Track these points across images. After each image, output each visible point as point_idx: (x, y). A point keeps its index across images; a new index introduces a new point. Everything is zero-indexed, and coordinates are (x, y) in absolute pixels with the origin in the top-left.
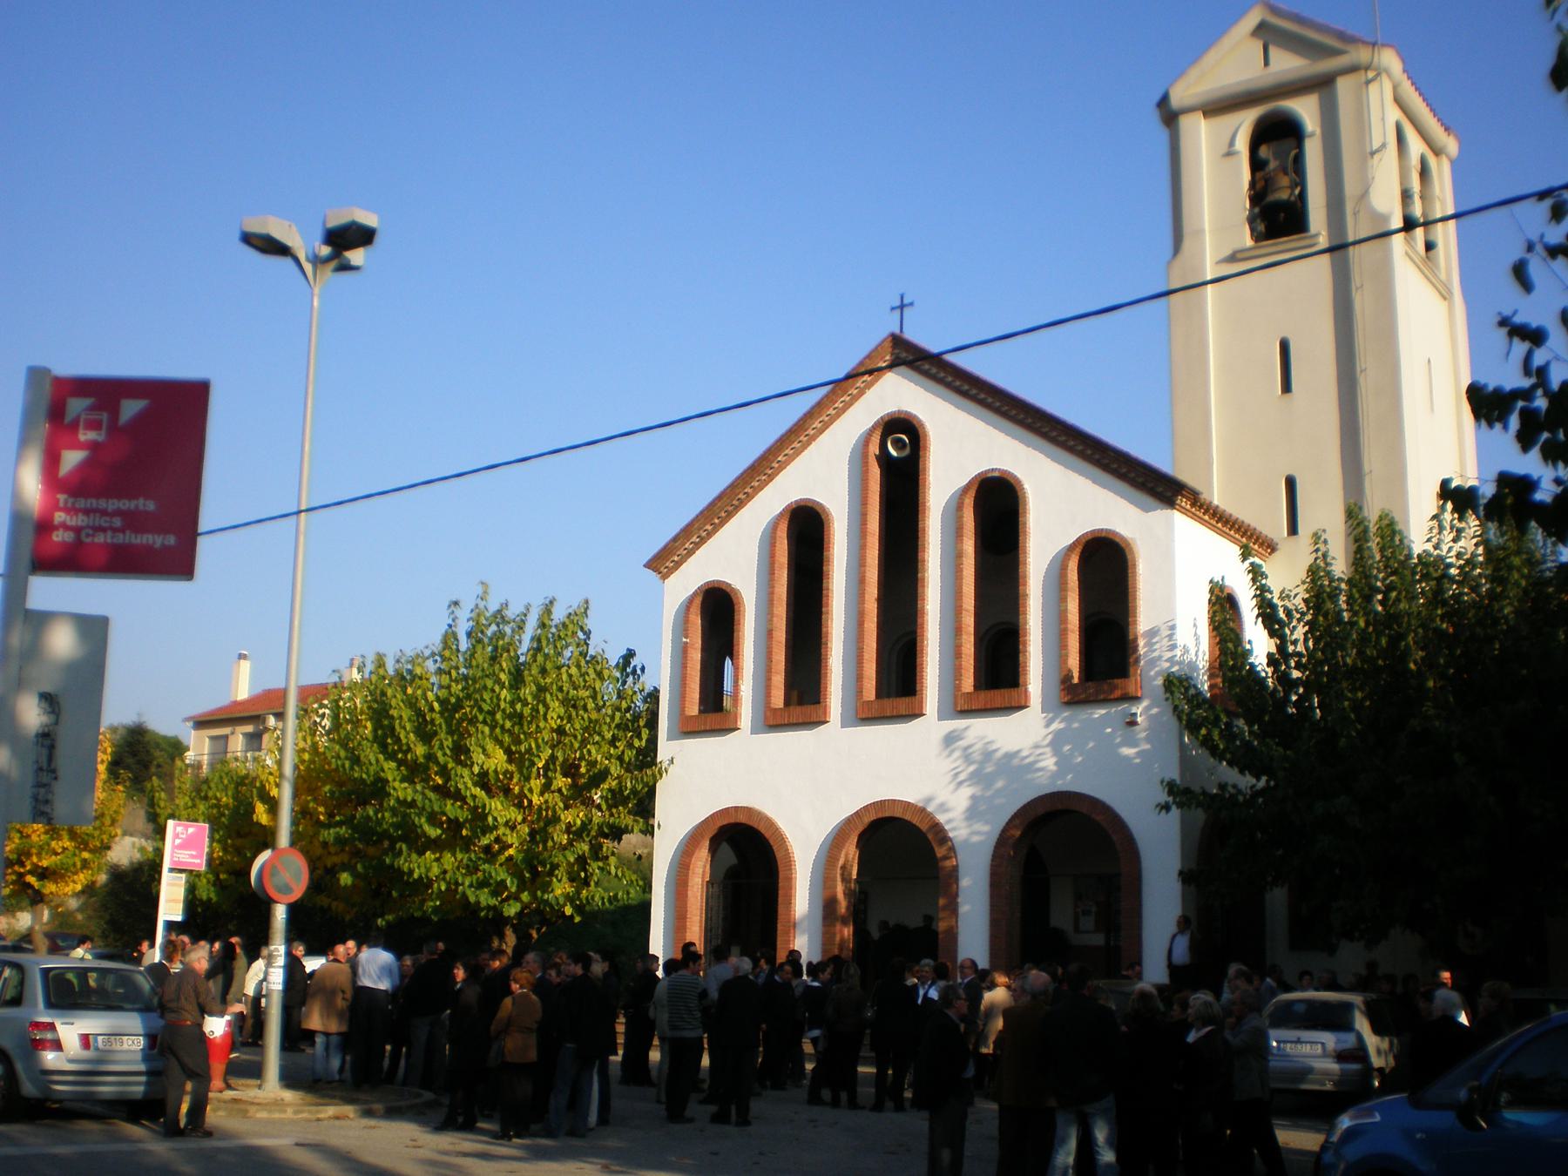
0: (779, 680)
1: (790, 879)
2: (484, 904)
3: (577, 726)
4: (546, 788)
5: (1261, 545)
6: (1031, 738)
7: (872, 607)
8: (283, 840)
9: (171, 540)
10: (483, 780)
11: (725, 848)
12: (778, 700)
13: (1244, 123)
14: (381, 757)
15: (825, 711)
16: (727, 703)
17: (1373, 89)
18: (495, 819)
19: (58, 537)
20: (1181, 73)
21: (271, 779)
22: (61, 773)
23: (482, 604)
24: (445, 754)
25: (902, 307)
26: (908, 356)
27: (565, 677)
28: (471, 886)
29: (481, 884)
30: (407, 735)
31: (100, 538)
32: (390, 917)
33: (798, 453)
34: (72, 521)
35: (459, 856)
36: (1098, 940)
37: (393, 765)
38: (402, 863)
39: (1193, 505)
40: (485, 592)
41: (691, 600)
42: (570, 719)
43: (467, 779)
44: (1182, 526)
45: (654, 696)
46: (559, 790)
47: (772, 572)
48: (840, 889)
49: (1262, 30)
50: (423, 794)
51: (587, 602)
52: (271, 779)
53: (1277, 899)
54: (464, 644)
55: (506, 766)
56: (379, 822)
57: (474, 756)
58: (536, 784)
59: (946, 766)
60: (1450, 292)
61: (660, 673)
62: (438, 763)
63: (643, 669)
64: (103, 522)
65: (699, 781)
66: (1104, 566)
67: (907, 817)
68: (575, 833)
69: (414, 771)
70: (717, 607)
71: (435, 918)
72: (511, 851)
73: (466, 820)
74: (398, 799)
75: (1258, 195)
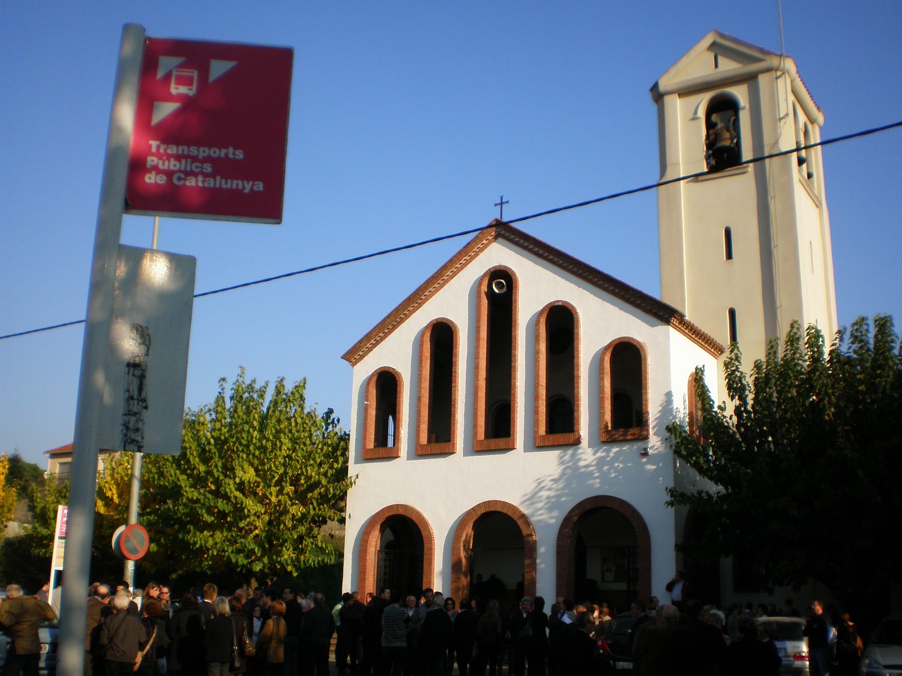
0: (424, 427)
1: (431, 549)
2: (240, 563)
3: (300, 455)
4: (280, 492)
5: (715, 349)
6: (592, 463)
7: (482, 383)
8: (133, 519)
9: (259, 186)
10: (241, 487)
11: (388, 531)
12: (424, 439)
13: (703, 101)
14: (178, 472)
15: (454, 445)
16: (390, 443)
17: (780, 82)
18: (249, 511)
19: (150, 179)
20: (666, 71)
21: (107, 485)
22: (150, 403)
23: (241, 380)
24: (218, 471)
25: (502, 204)
26: (504, 231)
27: (293, 424)
28: (232, 552)
29: (239, 551)
30: (195, 460)
31: (191, 182)
32: (180, 572)
33: (437, 290)
34: (163, 165)
35: (225, 534)
36: (622, 586)
37: (185, 477)
38: (190, 538)
39: (680, 323)
40: (243, 373)
41: (370, 379)
42: (294, 450)
43: (232, 486)
44: (674, 336)
45: (345, 438)
46: (288, 494)
47: (421, 362)
48: (463, 554)
49: (714, 46)
50: (204, 495)
51: (305, 379)
52: (107, 485)
53: (727, 564)
54: (228, 404)
55: (255, 478)
56: (175, 513)
57: (237, 472)
58: (274, 490)
59: (528, 479)
60: (821, 204)
61: (350, 421)
62: (213, 476)
63: (338, 420)
64: (195, 167)
65: (372, 490)
66: (626, 359)
67: (505, 511)
68: (297, 520)
69: (198, 481)
70: (386, 384)
71: (209, 572)
72: (257, 532)
73: (230, 512)
74: (188, 498)
75: (712, 143)
